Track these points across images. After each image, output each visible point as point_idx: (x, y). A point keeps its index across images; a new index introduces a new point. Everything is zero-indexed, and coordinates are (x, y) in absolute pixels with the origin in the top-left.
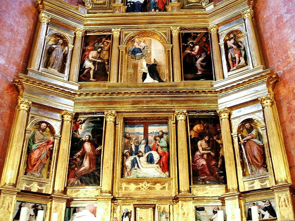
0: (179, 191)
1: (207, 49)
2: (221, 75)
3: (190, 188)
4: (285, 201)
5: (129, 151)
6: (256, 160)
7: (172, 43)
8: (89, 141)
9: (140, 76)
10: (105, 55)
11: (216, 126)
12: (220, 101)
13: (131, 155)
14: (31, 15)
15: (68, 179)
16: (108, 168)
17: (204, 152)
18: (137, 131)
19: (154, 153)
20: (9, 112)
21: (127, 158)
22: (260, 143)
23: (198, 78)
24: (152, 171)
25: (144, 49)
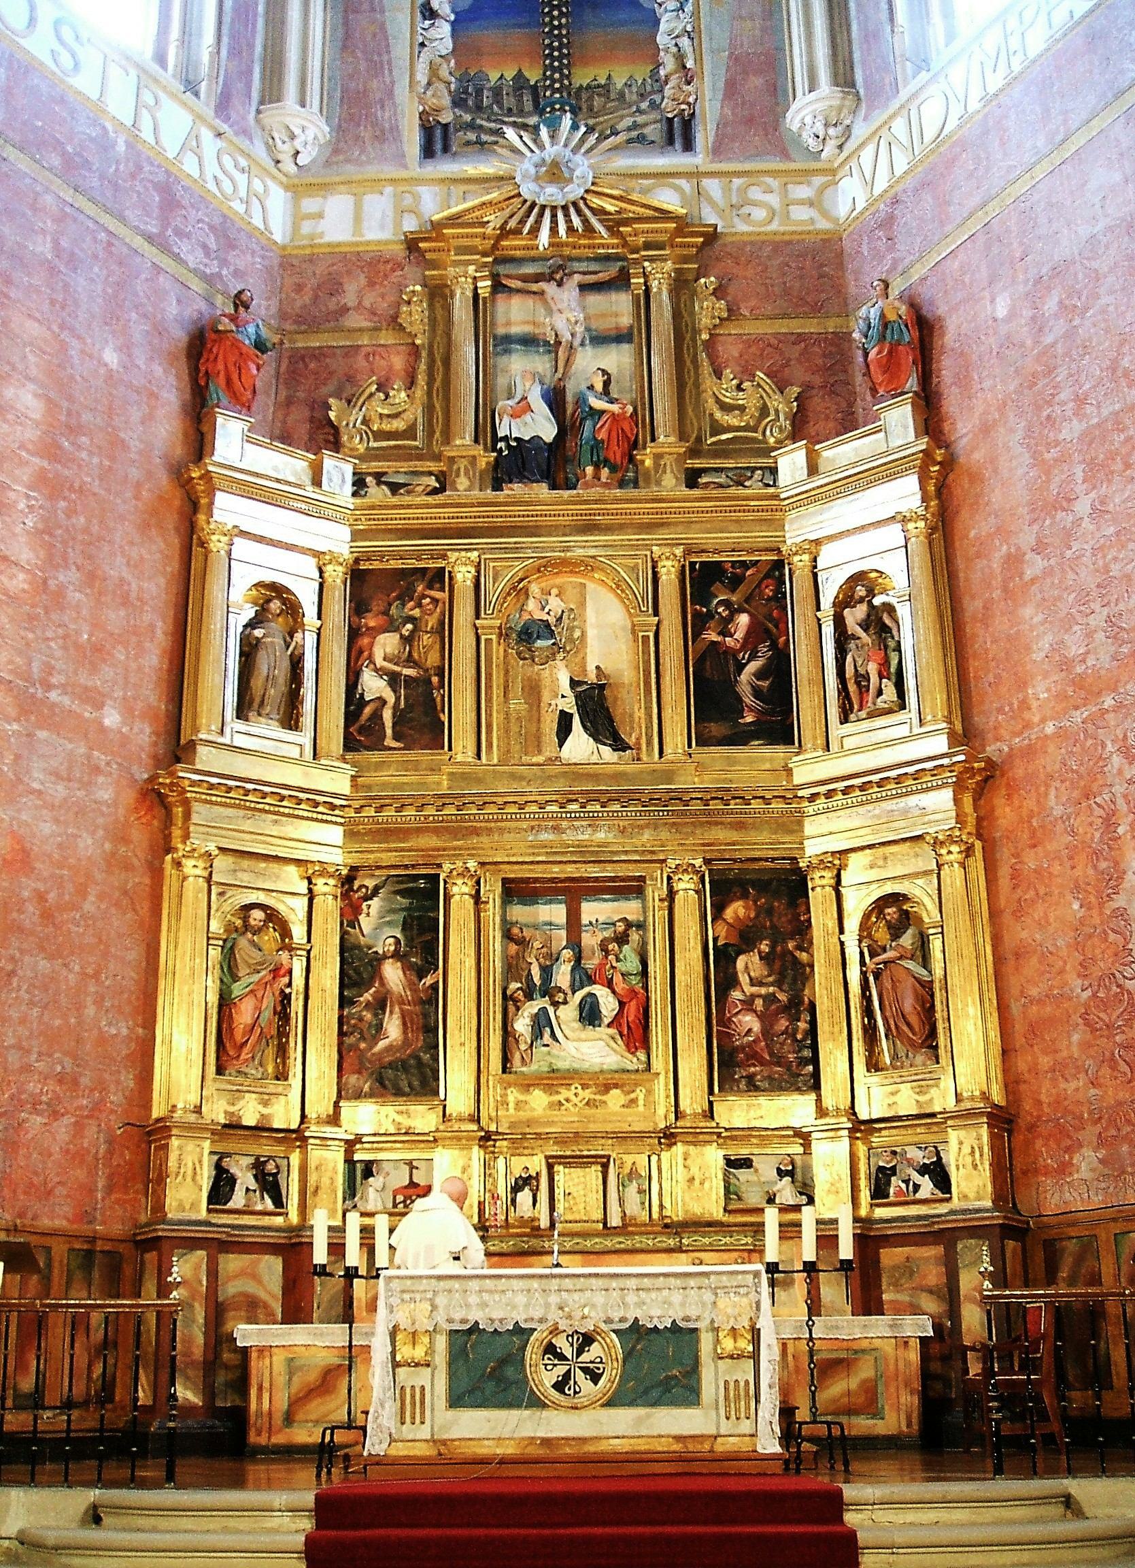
0: (678, 1115)
1: (777, 627)
2: (821, 741)
3: (711, 1103)
4: (973, 1152)
5: (523, 981)
6: (908, 1024)
7: (656, 613)
8: (396, 955)
9: (550, 725)
10: (428, 649)
11: (797, 906)
12: (810, 828)
13: (529, 997)
14: (171, 520)
15: (340, 1076)
16: (462, 1044)
17: (755, 989)
18: (547, 919)
19: (600, 991)
20: (147, 881)
21: (518, 1009)
22: (925, 972)
23: (739, 738)
24: (595, 1049)
25: (560, 619)
